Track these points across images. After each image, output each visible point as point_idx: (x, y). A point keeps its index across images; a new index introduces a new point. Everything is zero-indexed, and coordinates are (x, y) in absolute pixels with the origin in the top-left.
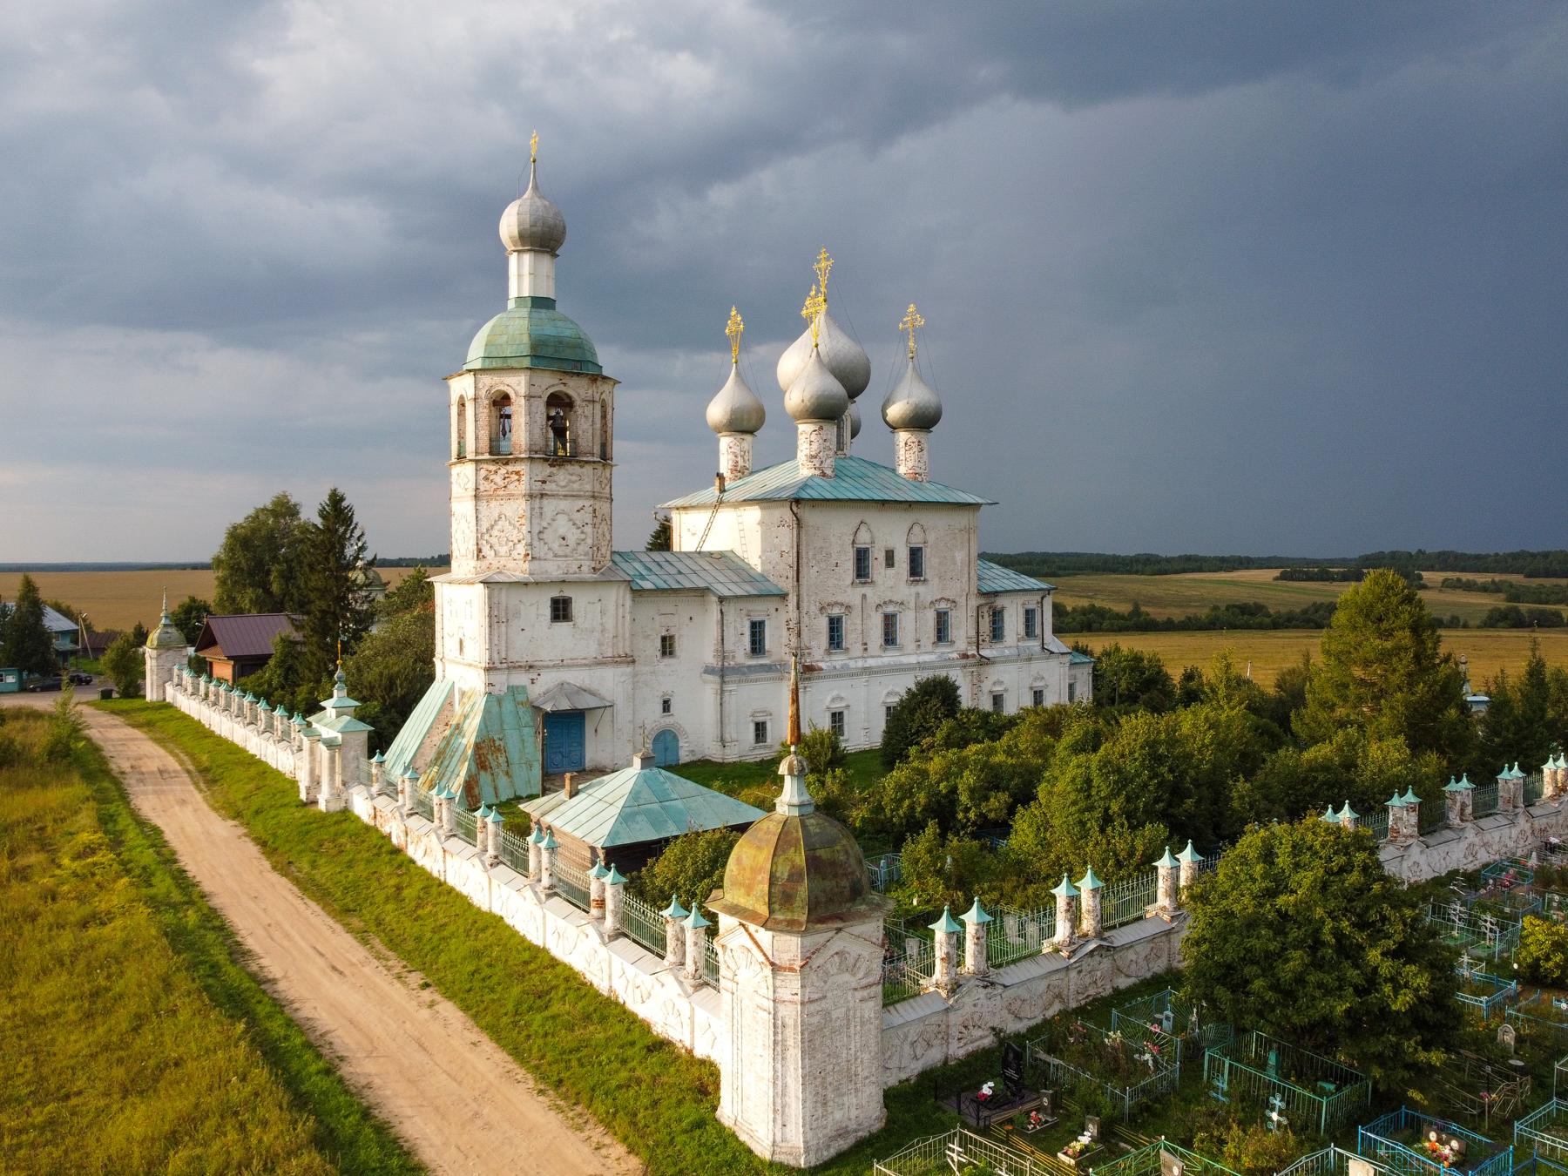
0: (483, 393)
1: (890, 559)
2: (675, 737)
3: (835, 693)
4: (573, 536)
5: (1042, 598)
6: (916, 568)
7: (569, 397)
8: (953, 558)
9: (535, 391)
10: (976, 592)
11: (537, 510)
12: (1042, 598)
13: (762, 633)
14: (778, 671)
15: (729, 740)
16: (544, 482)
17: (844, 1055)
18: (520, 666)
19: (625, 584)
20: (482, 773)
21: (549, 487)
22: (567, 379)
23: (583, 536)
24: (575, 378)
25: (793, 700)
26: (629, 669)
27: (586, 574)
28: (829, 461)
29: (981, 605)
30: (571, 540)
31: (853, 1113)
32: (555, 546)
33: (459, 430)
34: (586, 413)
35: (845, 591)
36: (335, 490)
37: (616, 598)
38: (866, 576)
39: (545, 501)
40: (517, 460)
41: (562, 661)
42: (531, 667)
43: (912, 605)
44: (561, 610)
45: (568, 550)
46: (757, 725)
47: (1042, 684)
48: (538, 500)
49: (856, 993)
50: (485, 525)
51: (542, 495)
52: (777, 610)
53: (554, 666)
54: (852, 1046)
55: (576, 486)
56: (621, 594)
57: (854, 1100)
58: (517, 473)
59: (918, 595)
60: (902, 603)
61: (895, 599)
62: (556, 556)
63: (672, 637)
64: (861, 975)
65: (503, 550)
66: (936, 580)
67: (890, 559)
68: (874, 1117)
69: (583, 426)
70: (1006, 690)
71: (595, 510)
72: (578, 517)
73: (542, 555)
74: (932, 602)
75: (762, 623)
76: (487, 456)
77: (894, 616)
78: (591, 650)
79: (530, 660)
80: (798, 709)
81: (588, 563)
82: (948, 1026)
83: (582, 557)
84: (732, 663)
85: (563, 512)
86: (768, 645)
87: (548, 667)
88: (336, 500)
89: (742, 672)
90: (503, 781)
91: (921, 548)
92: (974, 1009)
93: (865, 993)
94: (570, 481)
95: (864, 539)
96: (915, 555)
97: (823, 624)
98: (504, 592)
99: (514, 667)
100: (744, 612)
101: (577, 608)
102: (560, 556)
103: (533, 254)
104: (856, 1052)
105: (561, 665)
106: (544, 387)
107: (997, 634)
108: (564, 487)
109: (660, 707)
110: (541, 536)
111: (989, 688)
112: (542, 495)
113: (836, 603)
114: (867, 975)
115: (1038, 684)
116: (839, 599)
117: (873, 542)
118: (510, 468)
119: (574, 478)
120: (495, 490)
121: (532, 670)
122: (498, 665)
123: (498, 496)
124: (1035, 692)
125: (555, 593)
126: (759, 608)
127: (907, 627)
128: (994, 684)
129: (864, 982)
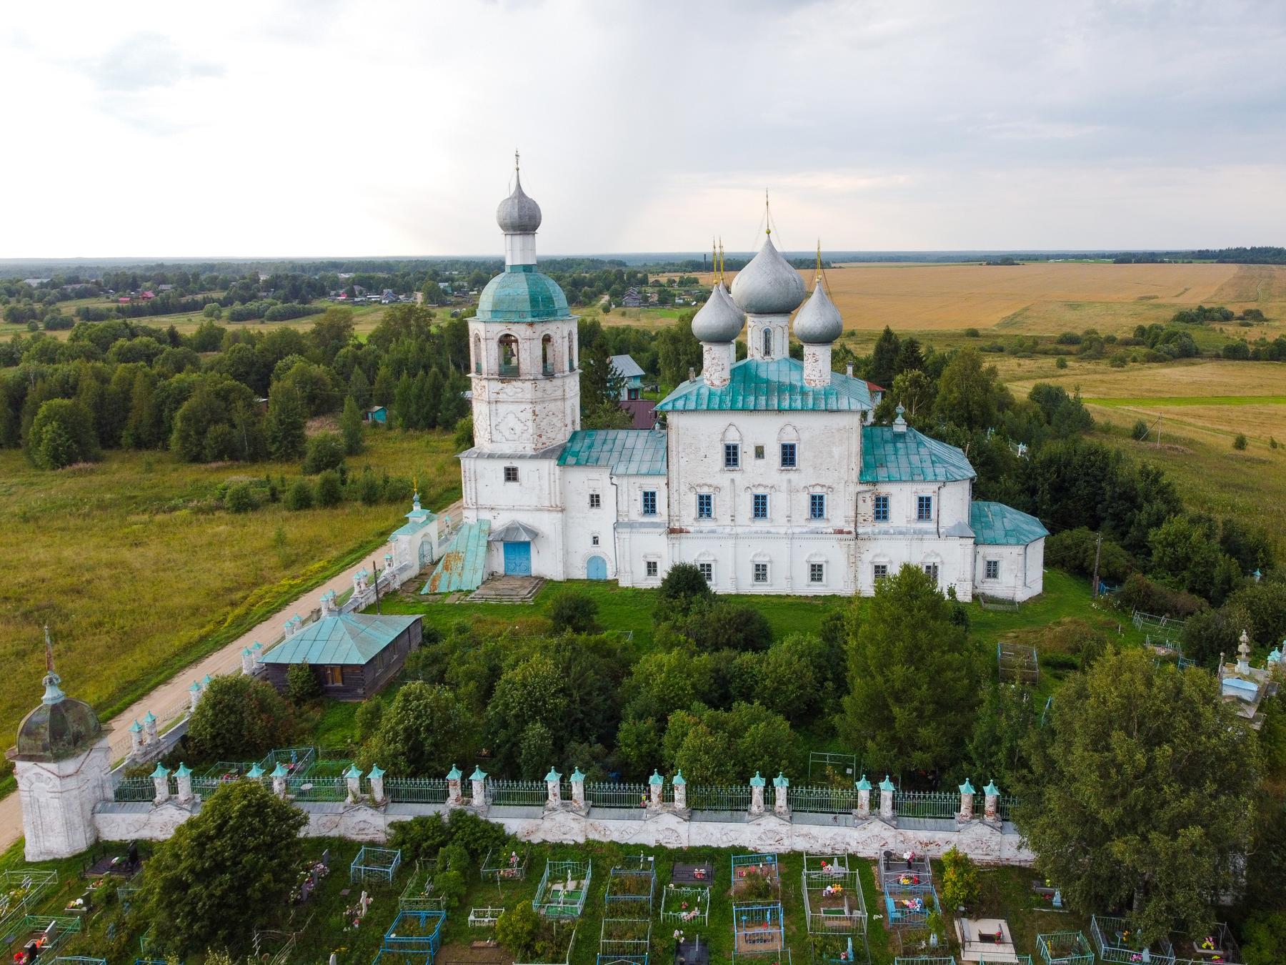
1: (760, 453)
4: (519, 428)
9: (489, 335)
10: (856, 480)
21: (502, 397)
22: (510, 326)
26: (560, 515)
32: (507, 433)
37: (549, 466)
39: (499, 405)
44: (511, 475)
45: (516, 437)
46: (649, 564)
55: (520, 395)
61: (765, 483)
63: (598, 496)
67: (760, 453)
71: (534, 412)
75: (653, 494)
78: (534, 502)
84: (626, 520)
85: (511, 412)
89: (631, 525)
90: (455, 578)
95: (732, 438)
97: (693, 501)
100: (637, 485)
101: (520, 474)
105: (512, 509)
107: (882, 509)
109: (591, 541)
111: (870, 559)
116: (709, 482)
117: (741, 440)
122: (470, 506)
125: (508, 464)
127: (776, 504)
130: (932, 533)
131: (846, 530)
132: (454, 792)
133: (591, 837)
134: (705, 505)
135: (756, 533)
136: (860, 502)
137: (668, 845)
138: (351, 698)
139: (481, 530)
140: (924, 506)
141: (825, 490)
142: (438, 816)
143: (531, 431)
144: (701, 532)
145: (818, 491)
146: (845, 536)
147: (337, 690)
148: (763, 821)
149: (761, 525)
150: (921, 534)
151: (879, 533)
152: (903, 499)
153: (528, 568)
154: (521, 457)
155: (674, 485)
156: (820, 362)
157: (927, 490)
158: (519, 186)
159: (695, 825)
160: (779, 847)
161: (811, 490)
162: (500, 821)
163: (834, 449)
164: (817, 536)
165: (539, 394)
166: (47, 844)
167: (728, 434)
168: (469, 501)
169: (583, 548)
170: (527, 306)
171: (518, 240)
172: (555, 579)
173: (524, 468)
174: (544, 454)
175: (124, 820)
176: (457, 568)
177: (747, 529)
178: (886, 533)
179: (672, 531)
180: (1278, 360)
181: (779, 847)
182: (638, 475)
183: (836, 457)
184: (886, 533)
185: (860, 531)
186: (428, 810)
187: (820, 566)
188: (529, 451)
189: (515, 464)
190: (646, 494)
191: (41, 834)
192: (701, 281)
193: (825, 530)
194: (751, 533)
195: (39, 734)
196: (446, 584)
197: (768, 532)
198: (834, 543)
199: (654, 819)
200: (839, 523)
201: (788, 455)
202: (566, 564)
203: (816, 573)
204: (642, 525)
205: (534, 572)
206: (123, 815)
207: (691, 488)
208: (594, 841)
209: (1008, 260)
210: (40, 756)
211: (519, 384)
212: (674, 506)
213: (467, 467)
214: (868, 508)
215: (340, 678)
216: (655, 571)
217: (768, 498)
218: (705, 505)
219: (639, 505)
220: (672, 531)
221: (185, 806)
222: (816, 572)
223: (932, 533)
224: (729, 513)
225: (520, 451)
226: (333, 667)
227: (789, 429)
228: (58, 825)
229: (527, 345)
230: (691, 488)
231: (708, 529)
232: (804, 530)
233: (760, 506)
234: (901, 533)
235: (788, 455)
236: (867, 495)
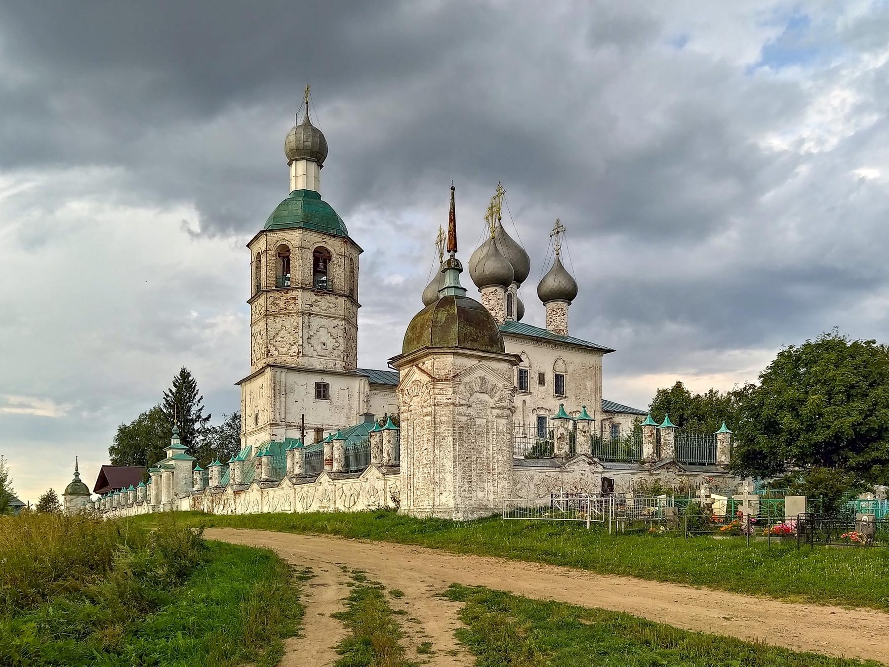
4: (331, 343)
6: (559, 389)
7: (329, 252)
8: (585, 385)
10: (600, 410)
16: (311, 306)
17: (485, 454)
19: (366, 378)
21: (315, 309)
22: (327, 239)
24: (332, 238)
25: (450, 218)
27: (339, 368)
29: (604, 420)
32: (319, 348)
33: (256, 278)
36: (184, 369)
39: (312, 318)
41: (322, 425)
45: (327, 353)
49: (493, 411)
50: (272, 333)
54: (491, 448)
55: (333, 310)
56: (362, 385)
57: (492, 488)
58: (294, 298)
60: (550, 410)
64: (497, 399)
66: (573, 399)
67: (542, 380)
69: (337, 272)
76: (274, 288)
80: (455, 226)
81: (340, 363)
82: (563, 482)
83: (337, 358)
88: (185, 375)
91: (563, 376)
93: (500, 412)
96: (559, 379)
98: (283, 374)
102: (322, 356)
108: (324, 310)
117: (530, 366)
118: (289, 295)
119: (332, 305)
120: (279, 311)
123: (281, 314)
129: (500, 404)
166: (480, 495)
173: (336, 385)
236: (607, 423)
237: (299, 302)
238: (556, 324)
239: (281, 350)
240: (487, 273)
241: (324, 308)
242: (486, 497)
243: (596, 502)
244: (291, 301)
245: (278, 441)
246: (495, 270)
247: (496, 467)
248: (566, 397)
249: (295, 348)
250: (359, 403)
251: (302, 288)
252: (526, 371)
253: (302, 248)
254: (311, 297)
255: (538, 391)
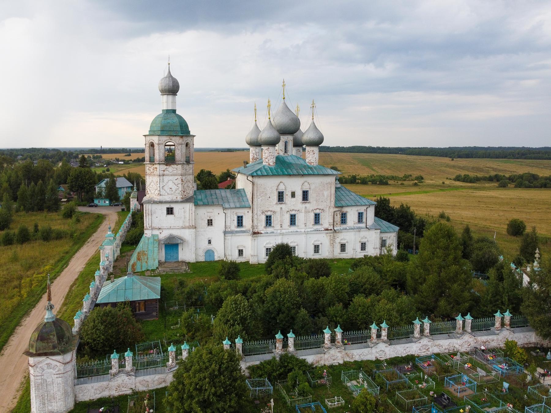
0: (147, 142)
1: (293, 195)
2: (213, 252)
3: (268, 242)
5: (367, 208)
8: (323, 194)
9: (160, 142)
10: (333, 206)
11: (162, 180)
12: (367, 208)
13: (242, 220)
14: (248, 232)
15: (228, 255)
16: (164, 171)
18: (156, 229)
20: (138, 261)
21: (166, 173)
23: (178, 188)
24: (175, 137)
26: (194, 230)
27: (179, 199)
28: (271, 160)
30: (174, 189)
31: (56, 408)
32: (168, 191)
34: (179, 148)
35: (273, 206)
38: (282, 201)
39: (164, 177)
40: (156, 164)
42: (159, 229)
43: (303, 211)
45: (173, 192)
46: (239, 250)
47: (366, 240)
48: (162, 177)
51: (163, 175)
52: (248, 212)
53: (167, 229)
54: (55, 389)
55: (175, 172)
56: (191, 206)
59: (306, 207)
60: (298, 211)
62: (168, 194)
63: (211, 220)
64: (56, 370)
65: (153, 192)
66: (315, 202)
67: (293, 195)
68: (63, 410)
70: (347, 242)
71: (182, 180)
72: (176, 182)
73: (164, 194)
74: (312, 210)
75: (242, 217)
77: (295, 215)
78: (181, 224)
79: (160, 227)
81: (180, 196)
84: (229, 230)
86: (244, 224)
87: (165, 229)
89: (232, 232)
90: (144, 264)
92: (122, 382)
93: (58, 376)
94: (173, 170)
95: (282, 188)
97: (263, 218)
99: (154, 229)
100: (235, 213)
101: (175, 211)
103: (166, 96)
104: (56, 392)
105: (170, 228)
106: (164, 141)
107: (344, 220)
109: (207, 242)
110: (163, 188)
111: (339, 241)
112: (163, 175)
113: (269, 211)
114: (58, 371)
115: (364, 241)
116: (270, 209)
117: (285, 189)
119: (175, 169)
121: (160, 230)
122: (148, 228)
124: (362, 244)
125: (168, 206)
126: (241, 211)
127: (300, 219)
128: (341, 240)
129: (58, 373)
130: (364, 228)
131: (329, 229)
132: (279, 345)
133: (345, 360)
134: (269, 221)
135: (292, 232)
136: (335, 216)
137: (381, 359)
138: (149, 318)
139: (154, 240)
140: (360, 215)
141: (321, 211)
142: (274, 358)
143: (180, 189)
144: (267, 233)
145: (318, 211)
146: (329, 231)
147: (142, 314)
148: (422, 341)
149: (293, 229)
150: (360, 229)
151: (343, 229)
152: (352, 215)
153: (177, 257)
154: (176, 202)
155: (255, 212)
156: (315, 154)
157: (362, 209)
158: (169, 72)
159: (393, 346)
160: (428, 352)
161: (315, 211)
162: (304, 357)
163: (325, 192)
164: (316, 232)
165: (184, 171)
166: (50, 408)
167: (279, 187)
168: (148, 226)
169: (204, 245)
170: (178, 129)
171: (170, 97)
172: (191, 262)
173: (177, 208)
174: (186, 200)
175: (92, 387)
176: (144, 259)
177: (287, 231)
178: (346, 229)
179: (254, 233)
180: (354, 183)
181: (428, 352)
182: (236, 208)
183: (326, 196)
184: (346, 229)
185: (335, 229)
186: (268, 357)
187: (318, 246)
188: (179, 199)
189: (172, 205)
190: (238, 217)
191: (46, 402)
192: (103, 157)
193: (320, 229)
194: (289, 232)
195: (50, 339)
196: (140, 268)
197: (297, 232)
198: (324, 235)
199: (376, 347)
200: (326, 226)
201: (305, 196)
202: (196, 254)
203: (317, 249)
204: (237, 232)
205: (180, 259)
206: (92, 385)
207: (263, 213)
208: (347, 361)
209: (229, 150)
210: (51, 352)
211: (175, 166)
212: (255, 221)
213: (147, 208)
214: (338, 218)
215: (143, 307)
216: (242, 254)
217: (297, 215)
218: (269, 221)
219: (235, 223)
220: (254, 233)
221: (132, 373)
222: (317, 249)
223: (364, 228)
224: (279, 224)
225: (174, 199)
226: (139, 302)
227: (306, 184)
228: (59, 395)
229: (180, 147)
230: (263, 213)
231: (270, 231)
232: (312, 230)
233: (293, 220)
234: (352, 229)
235: (305, 196)
236: (338, 213)
237: (158, 170)
238: (309, 159)
239: (152, 191)
240: (263, 140)
241: (171, 171)
242: (53, 408)
243: (314, 269)
244: (155, 169)
245: (148, 236)
246: (269, 136)
247: (57, 397)
248: (309, 202)
249: (157, 192)
250: (189, 215)
251: (158, 164)
252: (282, 193)
253: (159, 144)
254: (164, 167)
255: (291, 201)
